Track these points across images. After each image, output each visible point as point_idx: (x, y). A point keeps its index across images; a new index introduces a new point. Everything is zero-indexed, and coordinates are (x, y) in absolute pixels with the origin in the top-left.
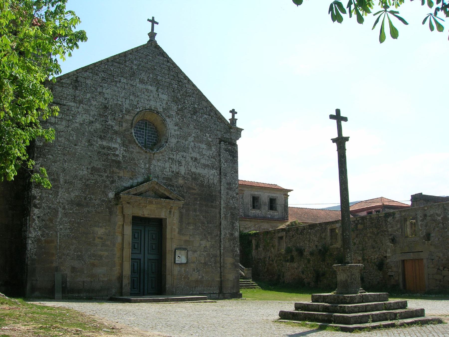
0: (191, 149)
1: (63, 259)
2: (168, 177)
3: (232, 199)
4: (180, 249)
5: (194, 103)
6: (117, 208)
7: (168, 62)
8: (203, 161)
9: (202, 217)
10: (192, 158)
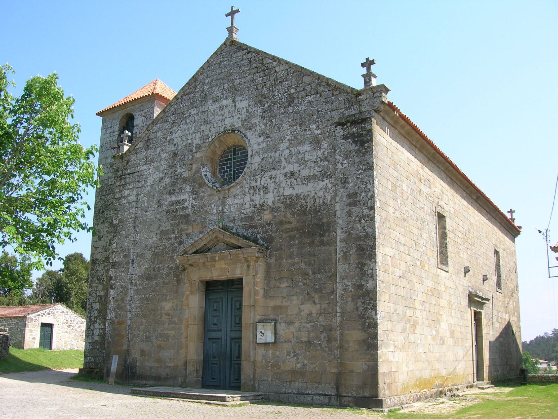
0: (284, 161)
1: (133, 341)
2: (248, 215)
3: (360, 221)
4: (264, 321)
5: (289, 88)
6: (185, 274)
7: (249, 53)
8: (305, 172)
9: (303, 266)
10: (285, 175)
